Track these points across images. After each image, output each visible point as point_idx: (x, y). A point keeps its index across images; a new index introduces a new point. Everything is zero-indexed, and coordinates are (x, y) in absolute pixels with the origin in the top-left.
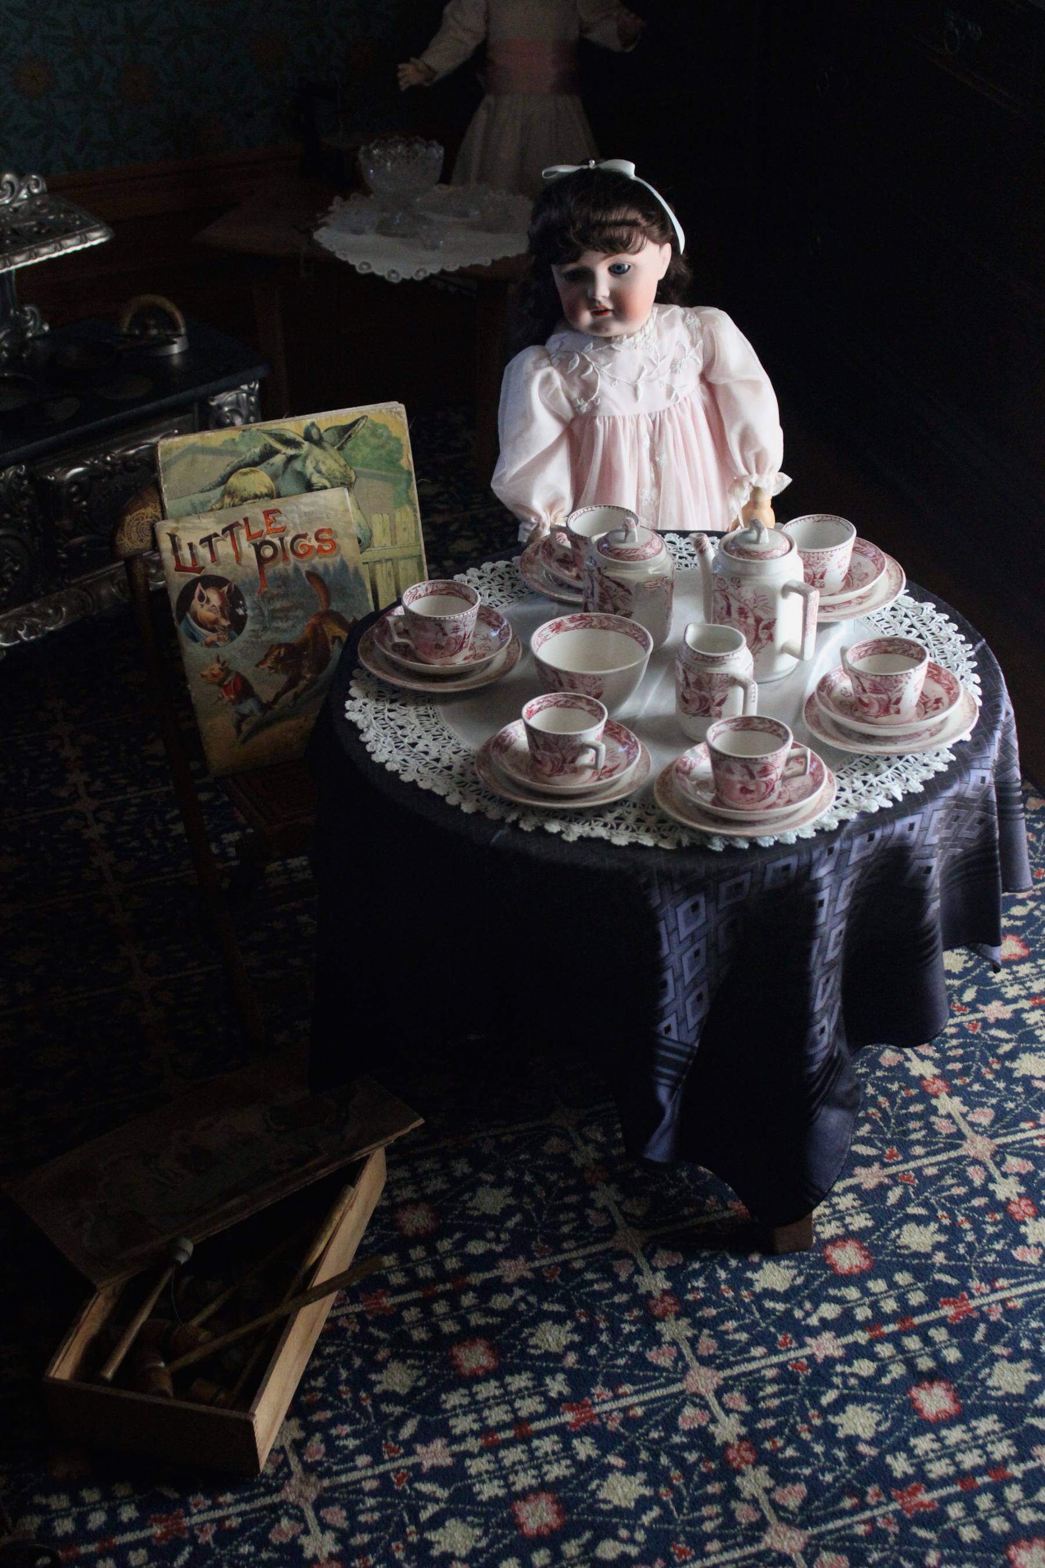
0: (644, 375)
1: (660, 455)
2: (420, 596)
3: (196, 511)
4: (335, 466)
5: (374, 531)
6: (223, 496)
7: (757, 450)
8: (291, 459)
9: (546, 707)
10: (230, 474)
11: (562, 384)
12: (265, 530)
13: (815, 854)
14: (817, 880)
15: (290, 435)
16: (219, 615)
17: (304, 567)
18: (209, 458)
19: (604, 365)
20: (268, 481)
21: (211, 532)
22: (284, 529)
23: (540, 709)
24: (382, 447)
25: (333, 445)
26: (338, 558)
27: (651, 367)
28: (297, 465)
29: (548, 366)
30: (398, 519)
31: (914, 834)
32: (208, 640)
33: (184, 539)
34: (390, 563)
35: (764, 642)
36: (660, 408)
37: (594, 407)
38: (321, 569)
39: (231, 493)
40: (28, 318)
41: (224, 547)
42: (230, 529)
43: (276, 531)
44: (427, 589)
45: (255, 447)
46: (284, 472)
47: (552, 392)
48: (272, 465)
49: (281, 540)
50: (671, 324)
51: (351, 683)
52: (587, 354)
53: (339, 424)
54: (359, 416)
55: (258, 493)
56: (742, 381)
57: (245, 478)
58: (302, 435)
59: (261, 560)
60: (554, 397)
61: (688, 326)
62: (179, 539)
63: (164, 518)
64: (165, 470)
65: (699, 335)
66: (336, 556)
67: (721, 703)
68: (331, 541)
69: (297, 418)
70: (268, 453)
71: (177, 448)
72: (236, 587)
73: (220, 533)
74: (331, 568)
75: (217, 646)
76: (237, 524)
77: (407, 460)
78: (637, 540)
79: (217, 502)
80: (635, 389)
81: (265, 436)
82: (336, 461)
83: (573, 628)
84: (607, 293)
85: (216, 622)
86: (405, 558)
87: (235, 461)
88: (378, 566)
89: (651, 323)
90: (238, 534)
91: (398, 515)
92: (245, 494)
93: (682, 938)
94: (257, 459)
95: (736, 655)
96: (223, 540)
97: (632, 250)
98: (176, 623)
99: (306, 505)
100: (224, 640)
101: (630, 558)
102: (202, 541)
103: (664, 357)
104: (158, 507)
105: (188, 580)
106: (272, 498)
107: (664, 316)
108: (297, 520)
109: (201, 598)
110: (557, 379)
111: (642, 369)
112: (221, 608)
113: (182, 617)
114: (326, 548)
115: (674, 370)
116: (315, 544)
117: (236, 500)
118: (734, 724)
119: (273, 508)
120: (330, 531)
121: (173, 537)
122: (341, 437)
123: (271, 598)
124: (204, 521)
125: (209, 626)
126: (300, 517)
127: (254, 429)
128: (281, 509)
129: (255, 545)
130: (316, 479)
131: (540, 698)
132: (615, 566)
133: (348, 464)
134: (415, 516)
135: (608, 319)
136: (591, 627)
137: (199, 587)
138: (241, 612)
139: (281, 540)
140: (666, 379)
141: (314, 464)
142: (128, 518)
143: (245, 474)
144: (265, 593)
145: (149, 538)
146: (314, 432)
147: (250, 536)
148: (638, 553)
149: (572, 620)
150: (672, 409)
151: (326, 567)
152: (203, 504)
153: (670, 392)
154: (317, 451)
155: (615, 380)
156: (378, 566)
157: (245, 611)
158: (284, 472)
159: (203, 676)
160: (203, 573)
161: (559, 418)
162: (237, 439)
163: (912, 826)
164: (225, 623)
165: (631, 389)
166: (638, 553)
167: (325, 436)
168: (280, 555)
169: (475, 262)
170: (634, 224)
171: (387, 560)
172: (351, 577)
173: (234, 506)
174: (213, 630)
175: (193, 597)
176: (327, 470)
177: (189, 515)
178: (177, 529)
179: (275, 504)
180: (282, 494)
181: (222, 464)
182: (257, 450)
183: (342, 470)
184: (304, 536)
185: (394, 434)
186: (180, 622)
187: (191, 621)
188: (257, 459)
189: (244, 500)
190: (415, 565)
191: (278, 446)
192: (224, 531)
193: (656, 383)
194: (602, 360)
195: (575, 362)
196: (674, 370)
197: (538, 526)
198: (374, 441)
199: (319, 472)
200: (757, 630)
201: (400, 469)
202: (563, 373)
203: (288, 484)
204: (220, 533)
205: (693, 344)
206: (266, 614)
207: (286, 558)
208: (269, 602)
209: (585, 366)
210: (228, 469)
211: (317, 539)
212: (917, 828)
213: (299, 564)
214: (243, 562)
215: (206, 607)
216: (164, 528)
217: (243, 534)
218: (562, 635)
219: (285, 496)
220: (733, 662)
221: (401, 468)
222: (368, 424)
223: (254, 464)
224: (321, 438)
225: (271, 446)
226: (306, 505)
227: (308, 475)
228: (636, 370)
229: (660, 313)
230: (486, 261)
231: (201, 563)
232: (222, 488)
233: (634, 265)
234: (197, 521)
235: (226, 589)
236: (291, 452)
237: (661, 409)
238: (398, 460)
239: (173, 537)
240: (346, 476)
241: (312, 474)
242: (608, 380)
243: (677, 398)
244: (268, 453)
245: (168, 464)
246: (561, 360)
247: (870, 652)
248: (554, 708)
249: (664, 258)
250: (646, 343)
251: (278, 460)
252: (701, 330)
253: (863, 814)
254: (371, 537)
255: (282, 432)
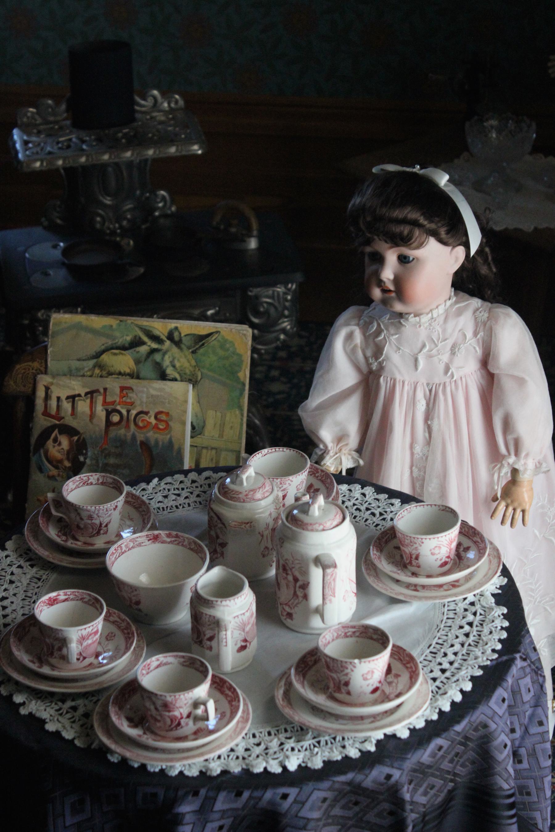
0: (425, 350)
1: (432, 419)
2: (91, 484)
3: (71, 373)
4: (187, 365)
5: (207, 423)
6: (94, 367)
7: (514, 436)
8: (153, 351)
9: (72, 600)
10: (103, 352)
11: (361, 342)
12: (118, 400)
13: (180, 793)
14: (178, 814)
15: (156, 333)
16: (64, 457)
17: (140, 437)
18: (90, 336)
19: (393, 335)
20: (132, 364)
21: (77, 392)
22: (132, 404)
23: (66, 600)
24: (227, 358)
25: (189, 348)
26: (168, 436)
27: (433, 346)
28: (157, 357)
29: (355, 325)
30: (227, 418)
31: (286, 805)
32: (51, 473)
33: (56, 392)
34: (214, 452)
35: (301, 599)
36: (437, 381)
37: (381, 368)
38: (152, 442)
39: (101, 367)
40: (159, 200)
41: (83, 406)
42: (91, 394)
43: (126, 403)
44: (98, 479)
45: (127, 335)
46: (146, 360)
47: (352, 345)
48: (138, 352)
49: (128, 411)
50: (459, 313)
51: (14, 537)
52: (383, 322)
53: (196, 332)
54: (214, 330)
55: (122, 371)
56: (507, 375)
57: (115, 358)
58: (166, 334)
59: (109, 423)
60: (354, 350)
61: (476, 319)
62: (52, 392)
63: (46, 373)
64: (53, 337)
65: (482, 328)
66: (167, 434)
67: (211, 639)
68: (167, 422)
69: (167, 320)
70: (136, 343)
71: (66, 323)
72: (84, 439)
73: (83, 395)
74: (161, 443)
75: (56, 480)
76: (97, 391)
77: (245, 374)
78: (245, 484)
79: (89, 370)
80: (416, 360)
81: (137, 329)
82: (189, 362)
83: (169, 543)
84: (391, 277)
85: (61, 461)
86: (227, 450)
87: (110, 342)
88: (204, 451)
89: (441, 310)
90: (96, 397)
91: (228, 415)
92: (112, 370)
93: (68, 824)
94: (127, 345)
95: (224, 603)
96: (84, 400)
97: (414, 245)
98: (31, 454)
99: (155, 389)
100: (62, 477)
101: (232, 499)
102: (68, 398)
103: (446, 340)
104: (43, 364)
105: (49, 424)
106: (132, 378)
107: (457, 306)
108: (144, 400)
109: (55, 440)
110: (358, 337)
111: (424, 346)
112: (68, 452)
113: (37, 450)
114: (161, 427)
115: (453, 352)
116: (153, 421)
117: (104, 373)
118: (182, 660)
119: (128, 385)
120: (167, 414)
121: (47, 389)
122: (196, 343)
123: (108, 455)
124: (73, 383)
125: (55, 463)
126: (148, 398)
127: (129, 322)
128: (134, 388)
129: (107, 410)
130: (170, 371)
131: (69, 591)
132: (222, 503)
133: (198, 365)
134: (242, 420)
135: (392, 298)
136: (183, 545)
137: (56, 431)
138: (82, 459)
139: (128, 411)
140: (445, 358)
141: (171, 359)
142: (18, 367)
143: (115, 354)
144: (105, 449)
145: (31, 385)
146: (176, 334)
147: (105, 403)
148: (240, 496)
149: (169, 536)
150: (447, 384)
151: (157, 442)
152: (78, 369)
153: (447, 369)
154: (175, 350)
155: (399, 349)
156: (204, 451)
157: (85, 459)
158: (146, 360)
159: (38, 500)
160: (62, 422)
161: (358, 368)
162: (114, 326)
163: (285, 796)
164: (67, 464)
165: (413, 360)
166: (240, 496)
167: (184, 339)
168: (124, 423)
169: (521, 226)
170: (415, 224)
171: (212, 449)
172: (175, 454)
173: (101, 377)
174: (57, 467)
175: (49, 438)
176: (181, 366)
177: (65, 375)
178: (52, 384)
179: (131, 382)
180: (141, 375)
181: (99, 343)
182: (129, 338)
183: (192, 369)
184: (147, 413)
185: (238, 351)
186: (34, 454)
187: (42, 455)
188: (127, 345)
189: (110, 374)
190: (234, 457)
191: (145, 339)
192: (87, 394)
193: (435, 359)
194: (392, 331)
195: (373, 327)
196: (453, 352)
197: (325, 452)
198: (221, 353)
199: (174, 366)
200: (295, 587)
201: (238, 380)
202: (364, 333)
203: (147, 370)
204: (83, 395)
205: (475, 334)
206: (100, 465)
207: (128, 426)
208: (105, 457)
209: (379, 332)
210: (103, 347)
211: (156, 418)
212: (290, 799)
213: (137, 434)
214: (95, 421)
215: (57, 448)
216: (43, 380)
217: (100, 399)
218: (157, 546)
219: (144, 379)
220: (221, 608)
221: (238, 378)
222: (220, 338)
223: (124, 348)
224: (180, 341)
225: (140, 338)
226: (155, 389)
227: (164, 367)
228: (419, 345)
229: (456, 302)
230: (528, 226)
231: (62, 414)
232: (95, 361)
233: (418, 259)
234: (68, 381)
235: (76, 438)
236: (154, 346)
237: (438, 382)
238: (237, 372)
239: (47, 389)
240: (194, 375)
241: (167, 366)
242: (395, 348)
243: (452, 376)
244: (136, 343)
245: (55, 334)
246: (365, 322)
247: (357, 634)
248: (79, 603)
249: (457, 259)
250: (430, 324)
251: (143, 349)
252: (485, 324)
253: (247, 772)
254: (203, 427)
255: (151, 329)
